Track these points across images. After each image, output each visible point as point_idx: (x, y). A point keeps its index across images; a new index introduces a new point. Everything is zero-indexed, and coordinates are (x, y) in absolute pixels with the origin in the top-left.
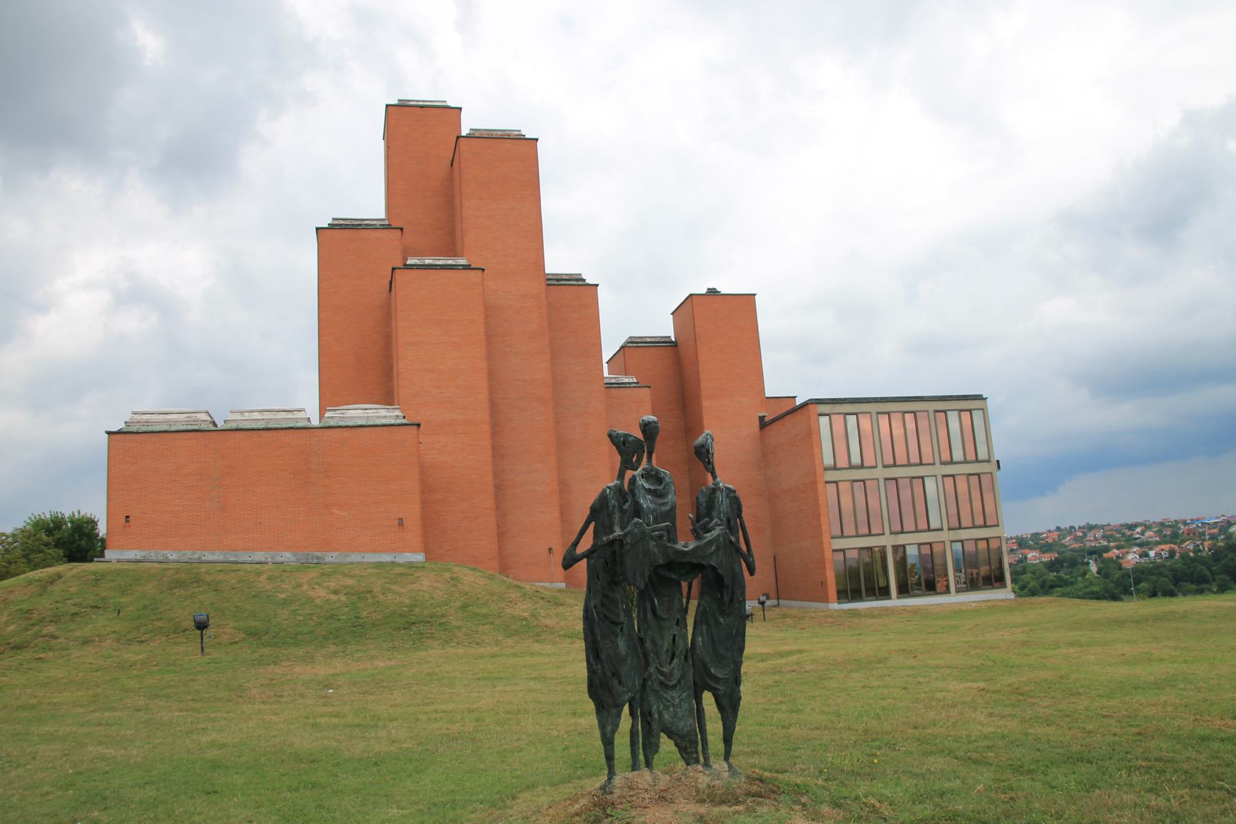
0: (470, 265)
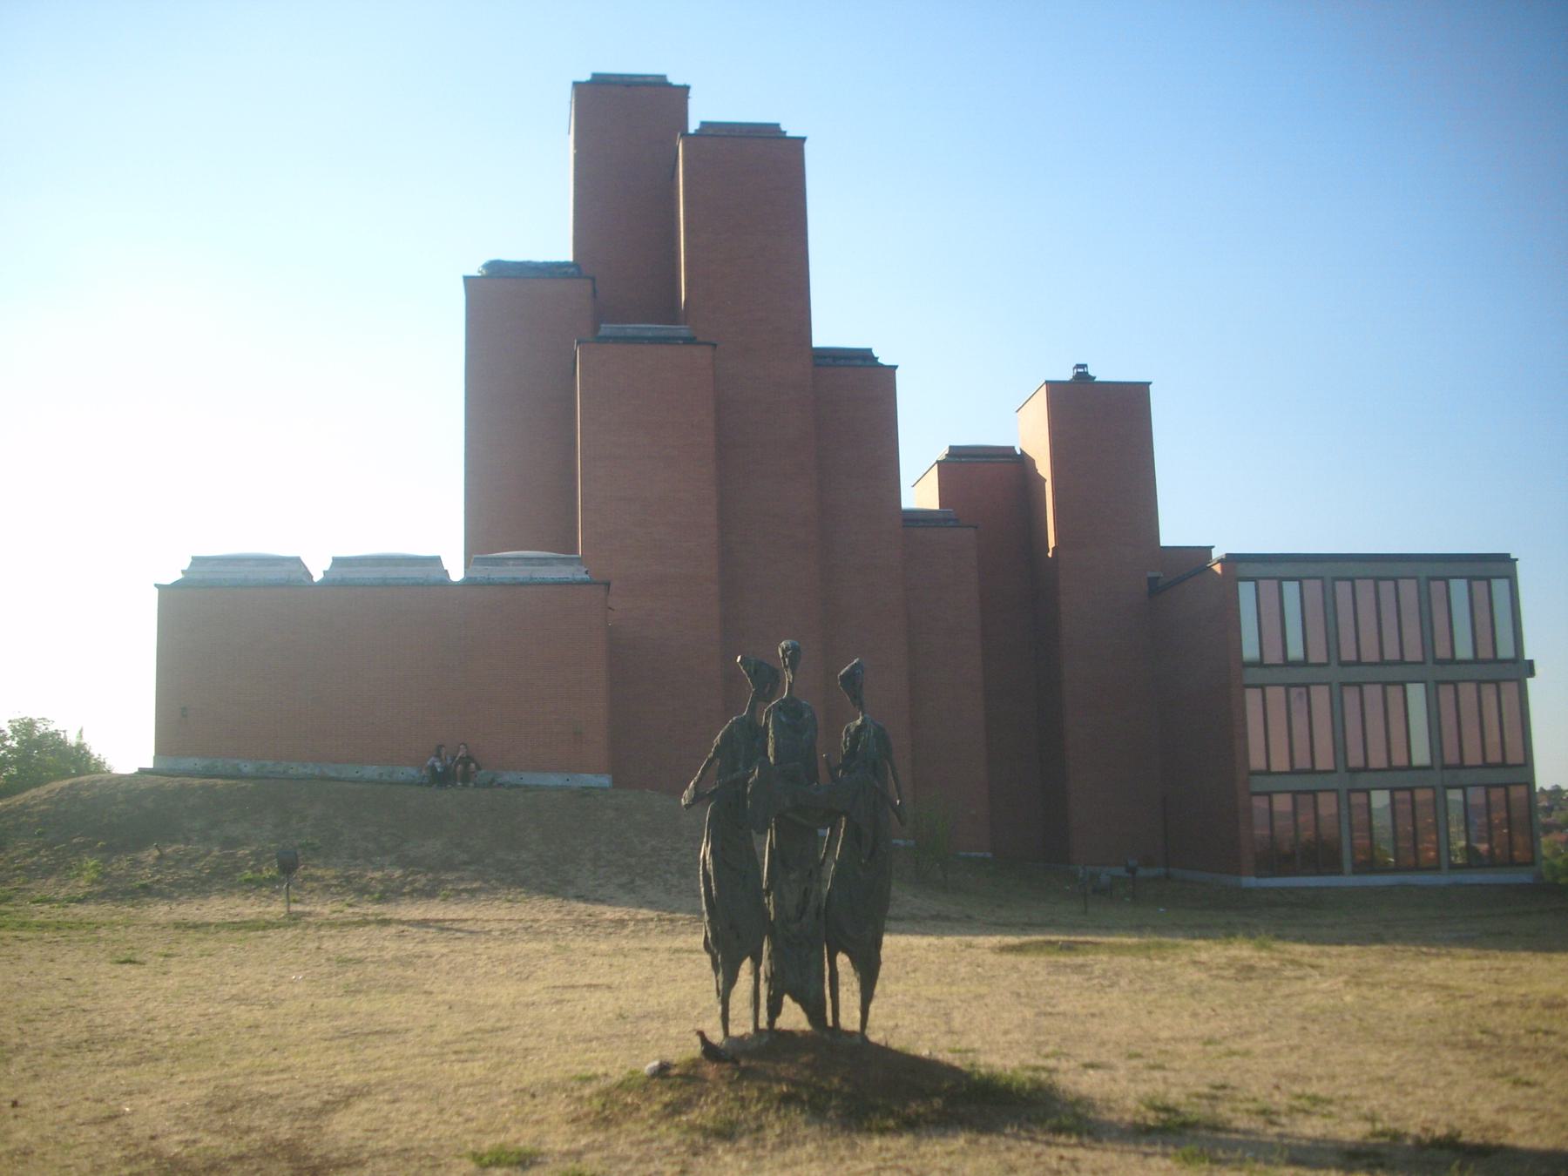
0: (695, 338)
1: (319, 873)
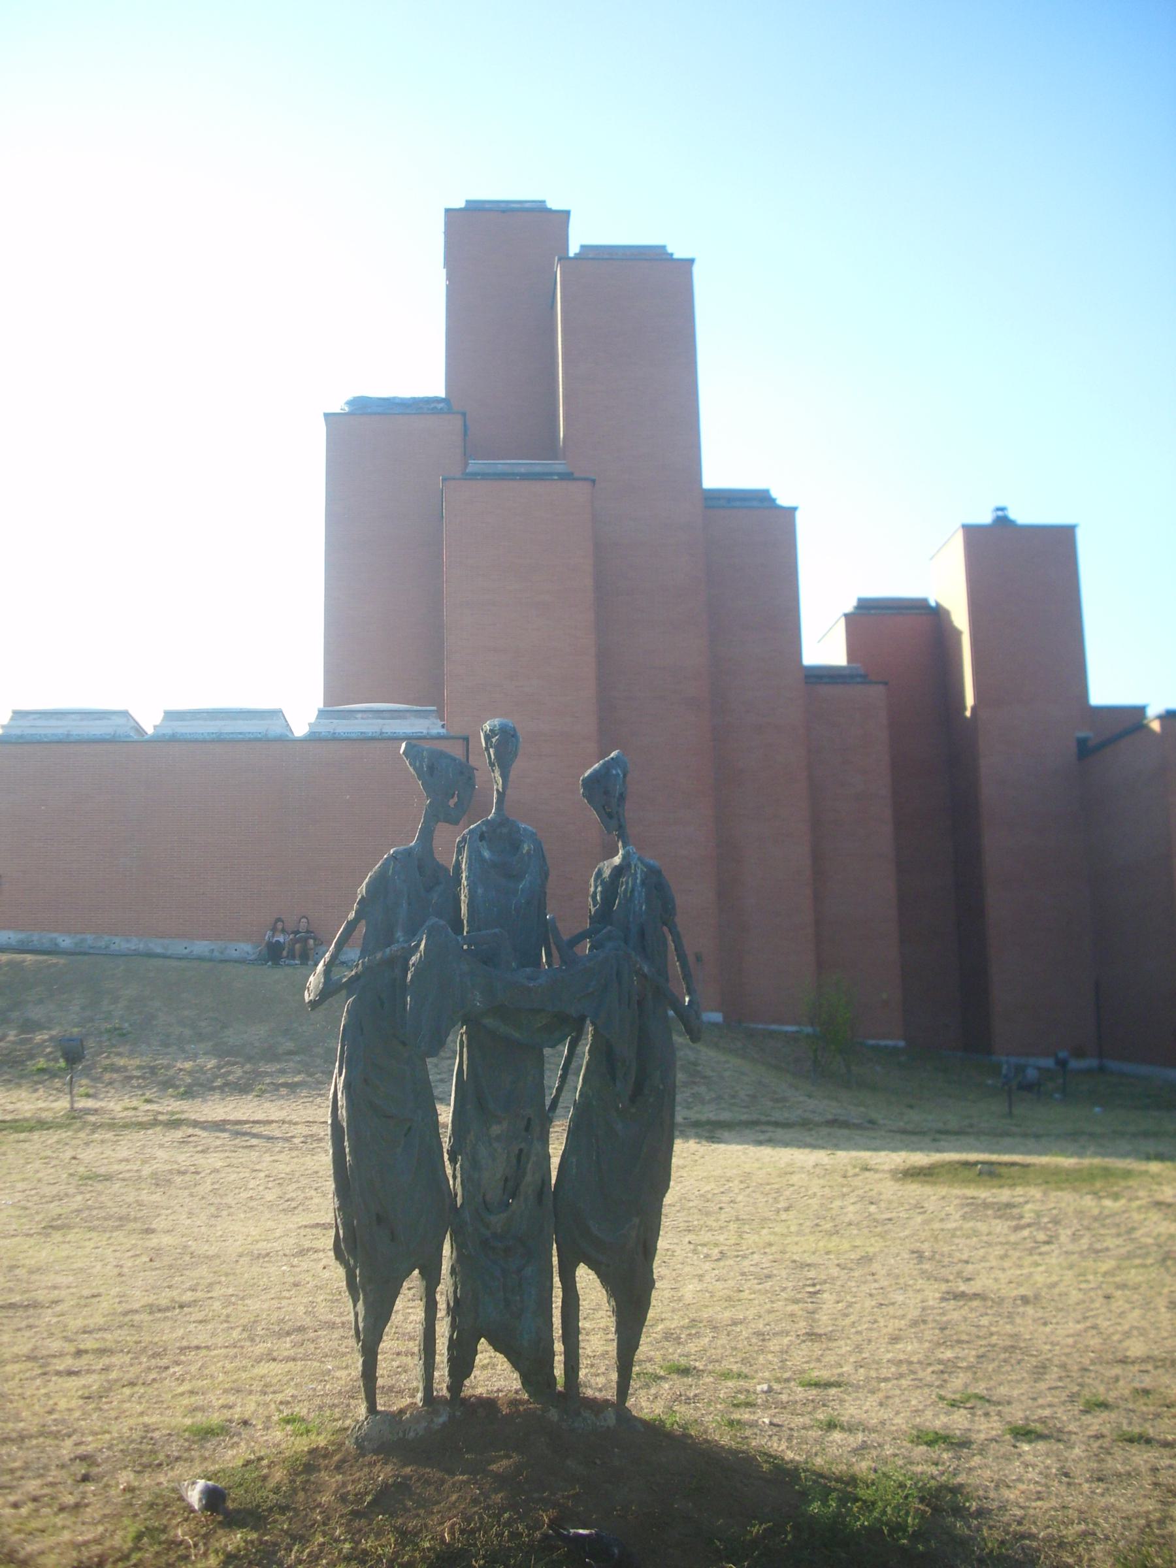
1: (121, 1062)
